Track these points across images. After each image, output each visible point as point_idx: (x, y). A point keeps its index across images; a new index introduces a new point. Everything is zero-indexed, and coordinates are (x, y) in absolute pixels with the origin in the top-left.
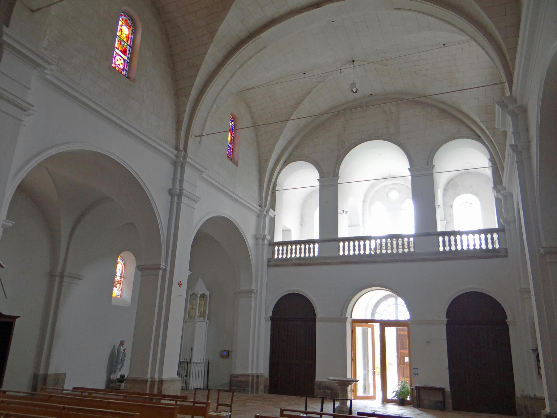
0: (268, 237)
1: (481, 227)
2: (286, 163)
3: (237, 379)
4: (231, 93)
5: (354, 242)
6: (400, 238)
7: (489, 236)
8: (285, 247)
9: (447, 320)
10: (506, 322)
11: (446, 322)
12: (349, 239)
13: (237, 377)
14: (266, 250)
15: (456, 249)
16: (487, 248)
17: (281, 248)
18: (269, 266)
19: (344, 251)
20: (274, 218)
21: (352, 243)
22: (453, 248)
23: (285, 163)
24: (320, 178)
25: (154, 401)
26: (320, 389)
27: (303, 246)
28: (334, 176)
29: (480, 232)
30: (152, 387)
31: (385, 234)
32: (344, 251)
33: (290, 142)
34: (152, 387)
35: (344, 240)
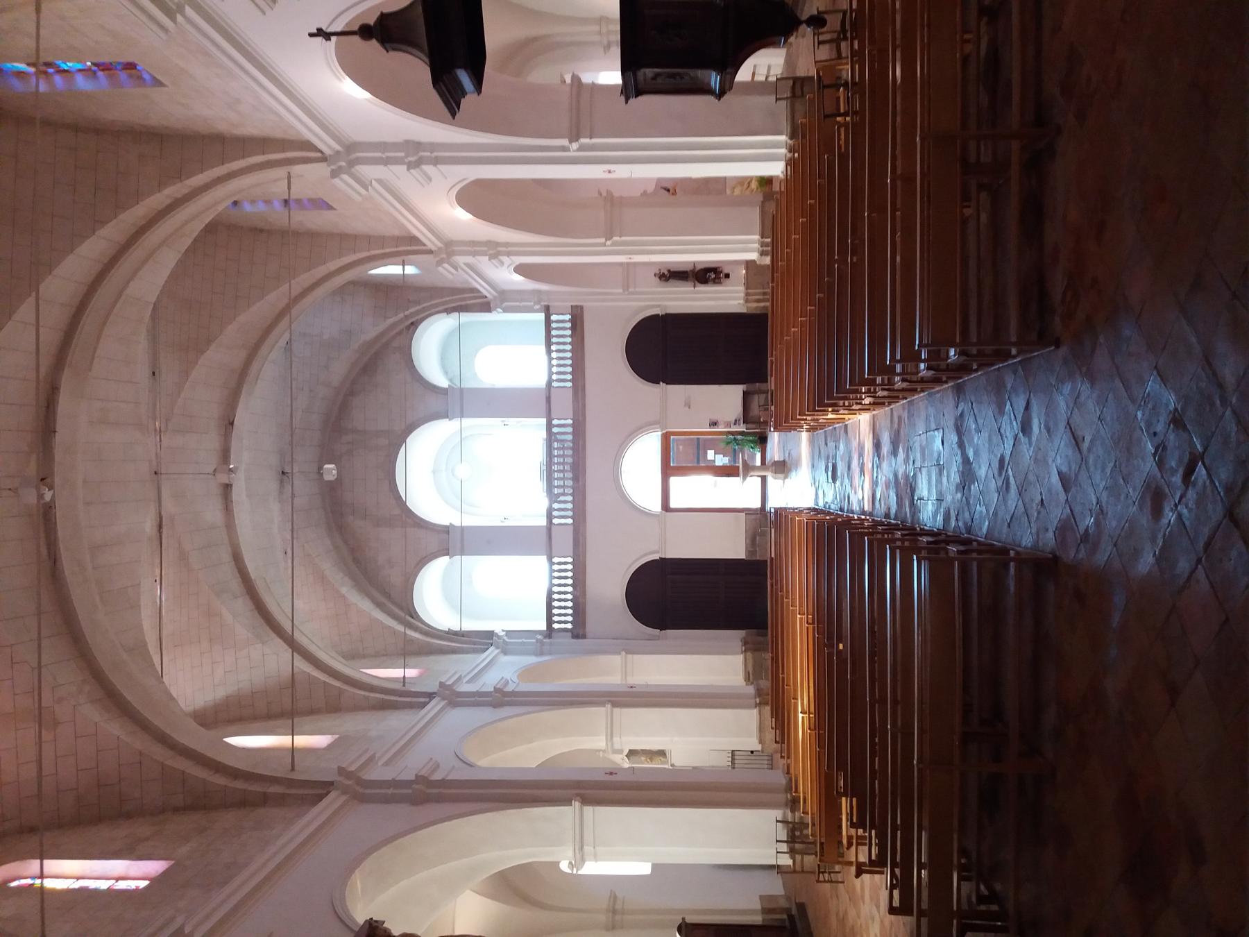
0: (540, 637)
1: (543, 348)
2: (413, 614)
3: (751, 672)
4: (253, 705)
5: (555, 615)
6: (551, 589)
7: (554, 340)
8: (554, 340)
9: (661, 383)
10: (662, 316)
11: (664, 385)
12: (550, 616)
13: (749, 673)
14: (560, 640)
15: (571, 578)
16: (571, 366)
17: (556, 618)
18: (584, 637)
19: (566, 622)
20: (507, 631)
21: (555, 611)
22: (570, 611)
23: (415, 617)
24: (448, 555)
25: (789, 250)
26: (756, 551)
27: (556, 604)
28: (448, 532)
29: (549, 351)
30: (767, 245)
31: (545, 358)
32: (566, 622)
33: (379, 605)
34: (767, 245)
35: (550, 622)
